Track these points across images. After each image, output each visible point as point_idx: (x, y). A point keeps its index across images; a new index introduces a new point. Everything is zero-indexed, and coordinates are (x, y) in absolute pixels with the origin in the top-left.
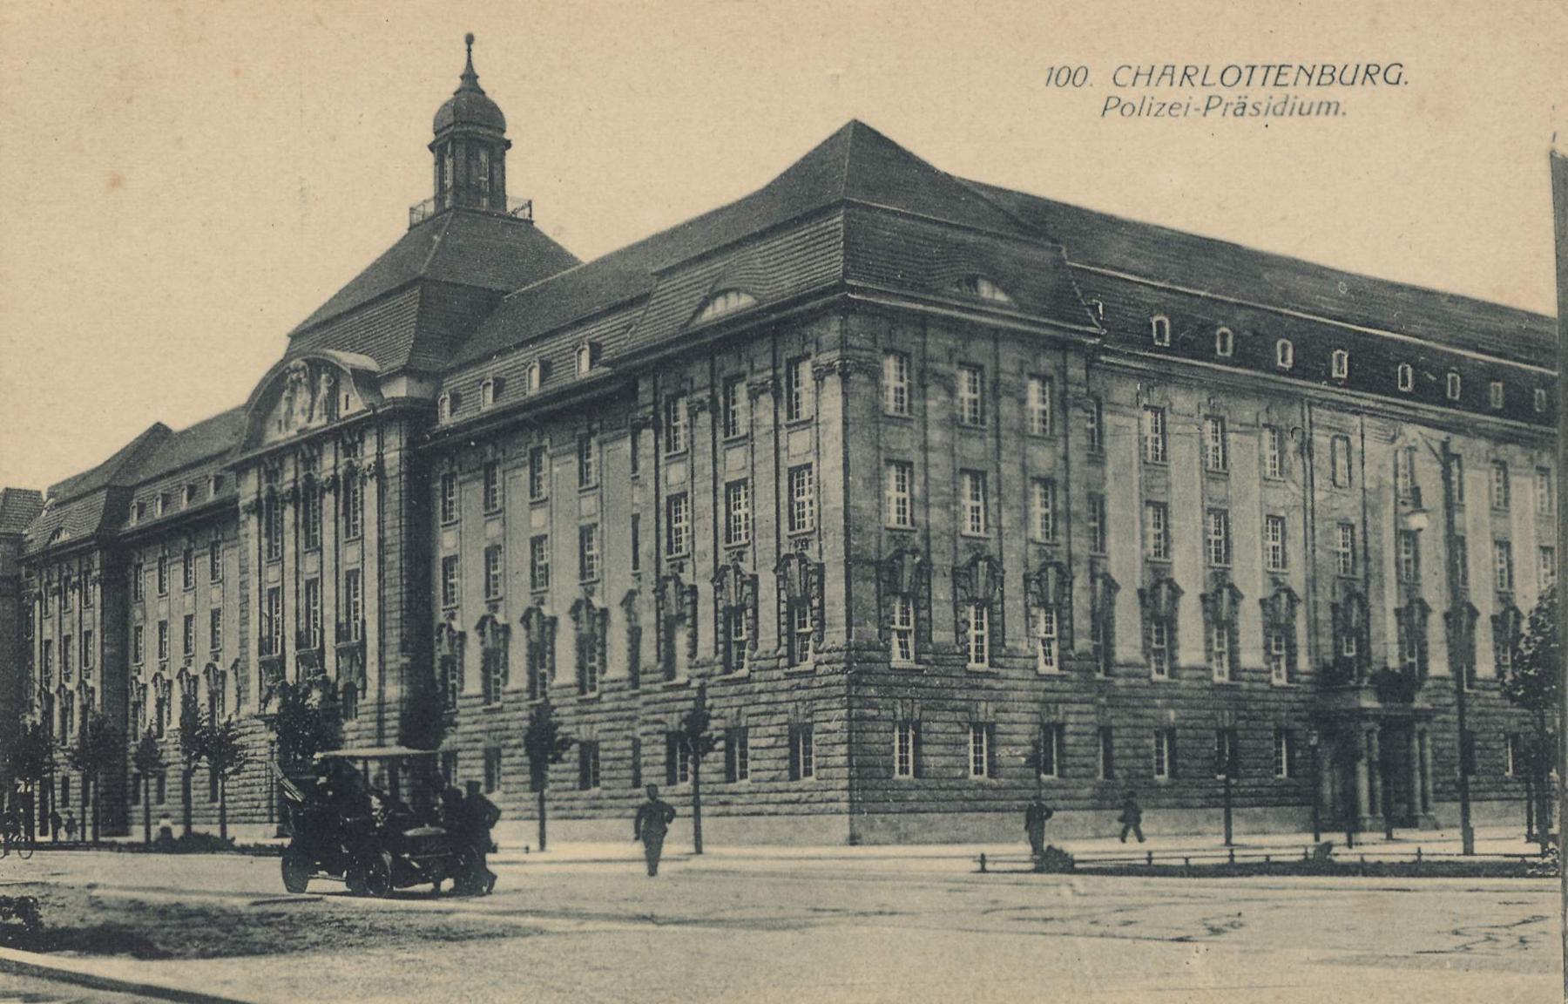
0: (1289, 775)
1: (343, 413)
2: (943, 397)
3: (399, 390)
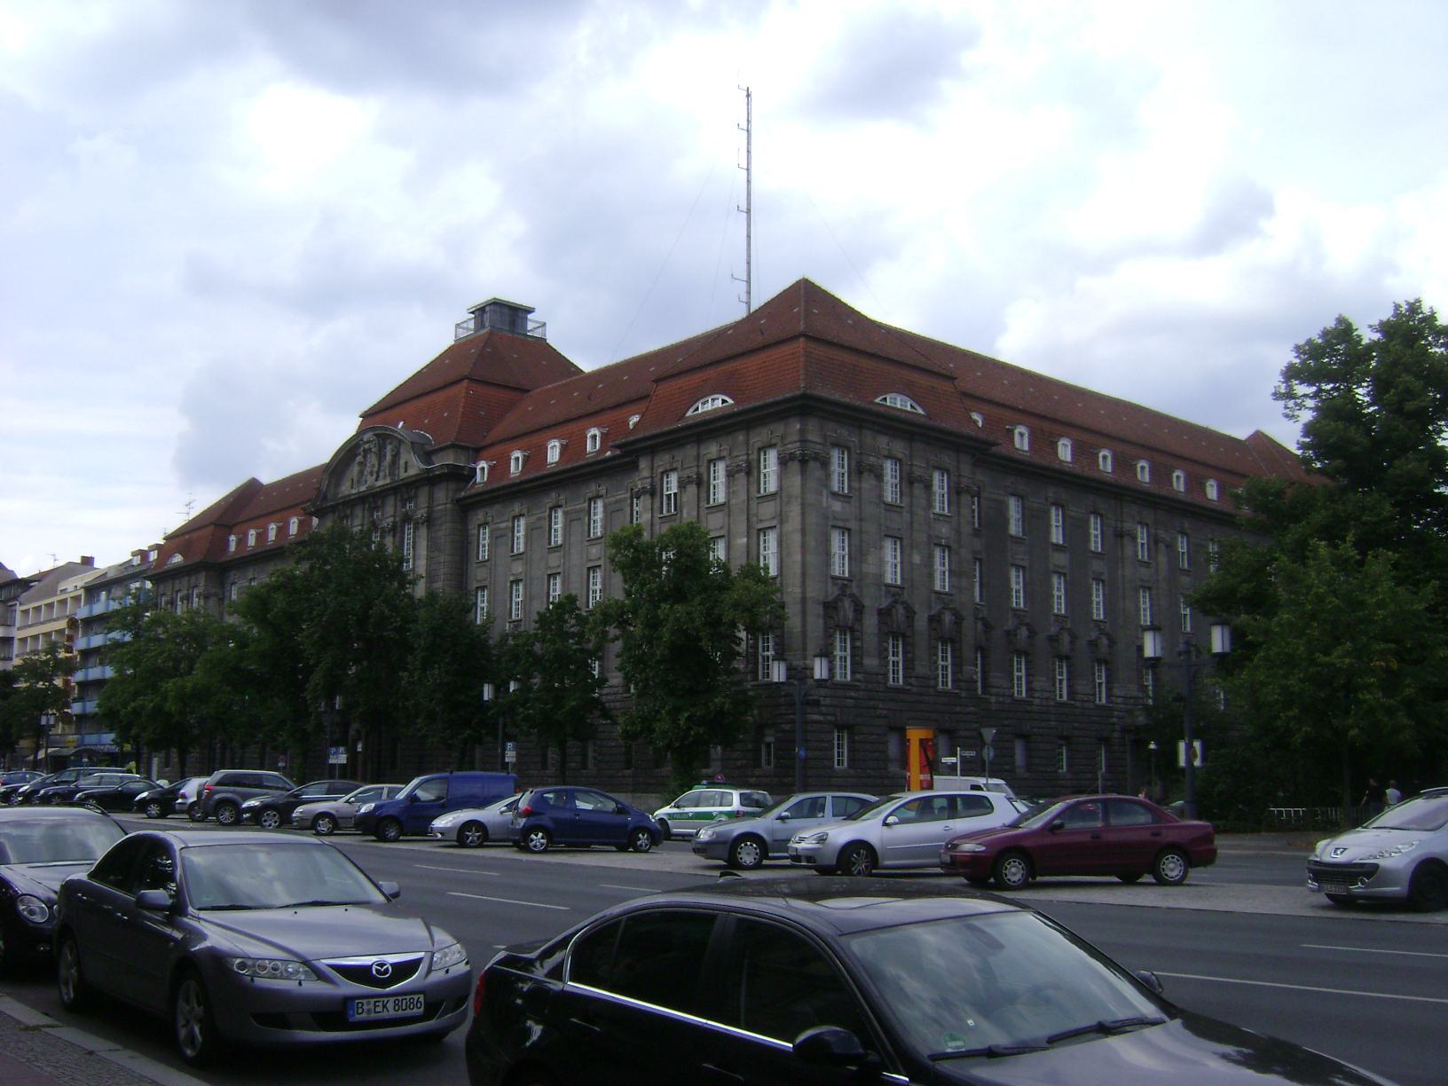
0: (850, 766)
1: (403, 475)
2: (874, 482)
3: (449, 459)
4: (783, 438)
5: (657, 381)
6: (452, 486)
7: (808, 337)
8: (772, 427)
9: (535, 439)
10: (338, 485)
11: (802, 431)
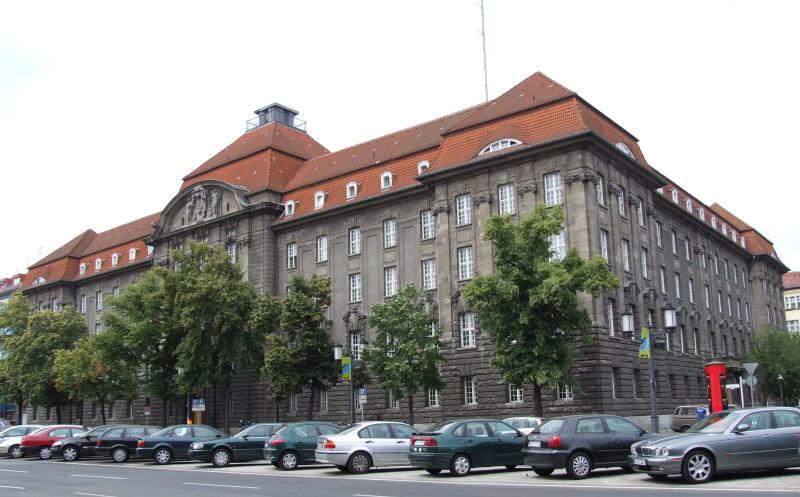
1: (225, 212)
4: (566, 166)
5: (445, 135)
6: (267, 217)
7: (70, 257)
8: (556, 158)
9: (90, 258)
10: (171, 223)
11: (583, 160)
